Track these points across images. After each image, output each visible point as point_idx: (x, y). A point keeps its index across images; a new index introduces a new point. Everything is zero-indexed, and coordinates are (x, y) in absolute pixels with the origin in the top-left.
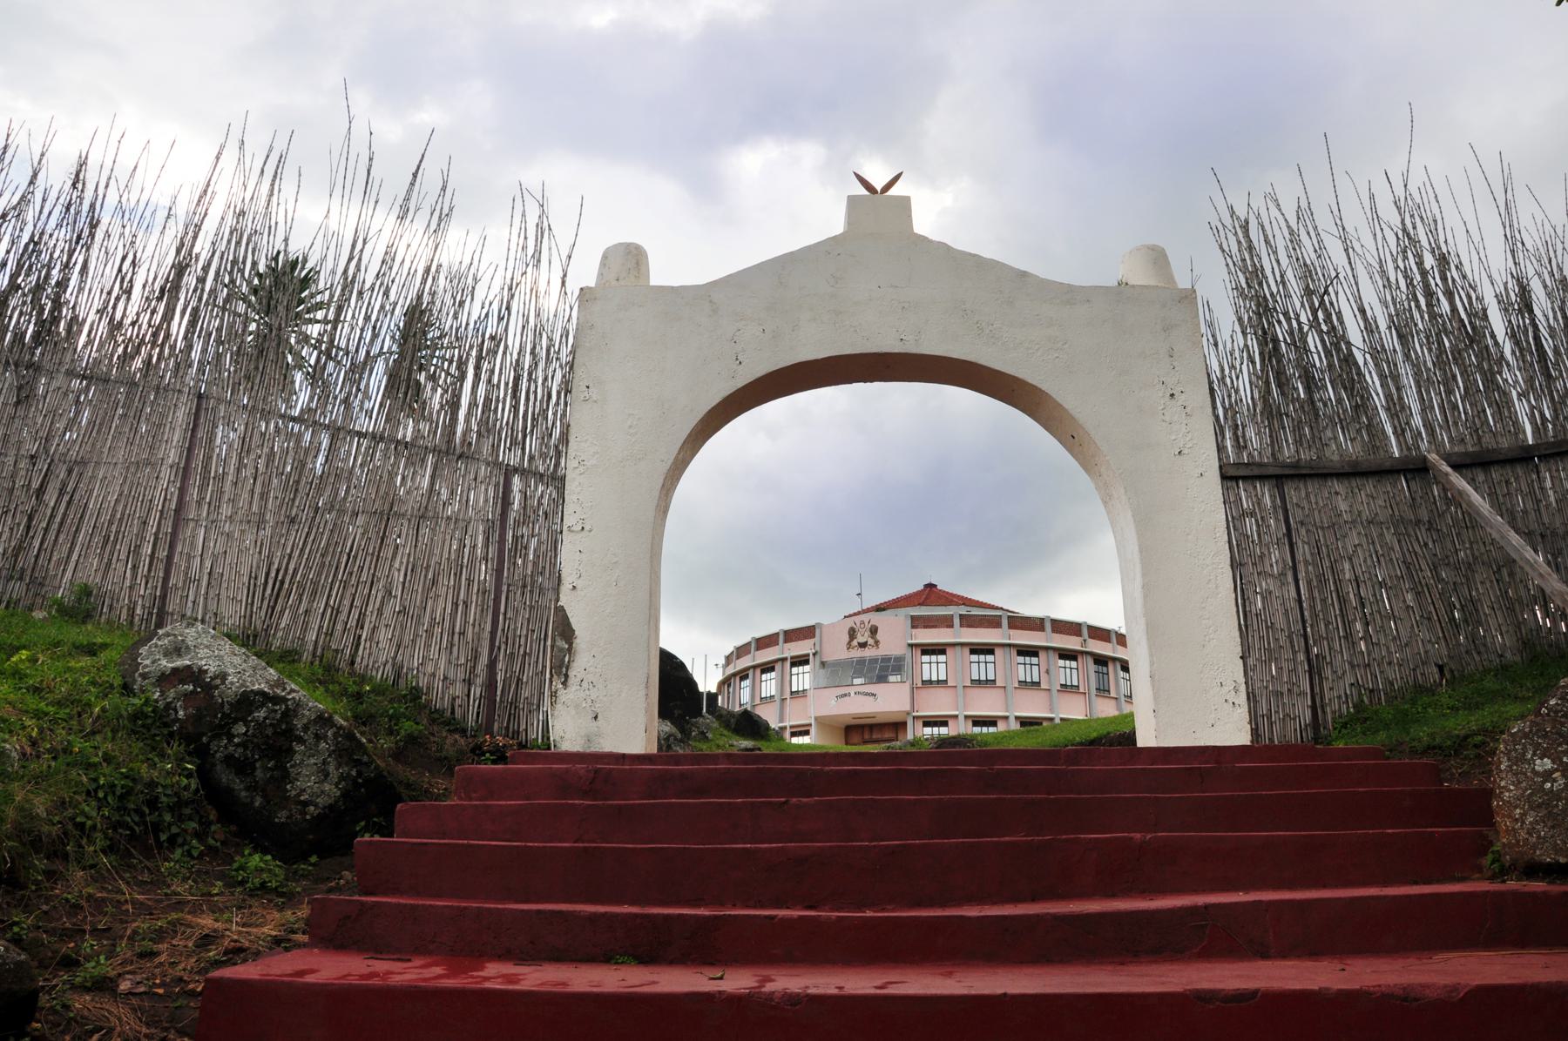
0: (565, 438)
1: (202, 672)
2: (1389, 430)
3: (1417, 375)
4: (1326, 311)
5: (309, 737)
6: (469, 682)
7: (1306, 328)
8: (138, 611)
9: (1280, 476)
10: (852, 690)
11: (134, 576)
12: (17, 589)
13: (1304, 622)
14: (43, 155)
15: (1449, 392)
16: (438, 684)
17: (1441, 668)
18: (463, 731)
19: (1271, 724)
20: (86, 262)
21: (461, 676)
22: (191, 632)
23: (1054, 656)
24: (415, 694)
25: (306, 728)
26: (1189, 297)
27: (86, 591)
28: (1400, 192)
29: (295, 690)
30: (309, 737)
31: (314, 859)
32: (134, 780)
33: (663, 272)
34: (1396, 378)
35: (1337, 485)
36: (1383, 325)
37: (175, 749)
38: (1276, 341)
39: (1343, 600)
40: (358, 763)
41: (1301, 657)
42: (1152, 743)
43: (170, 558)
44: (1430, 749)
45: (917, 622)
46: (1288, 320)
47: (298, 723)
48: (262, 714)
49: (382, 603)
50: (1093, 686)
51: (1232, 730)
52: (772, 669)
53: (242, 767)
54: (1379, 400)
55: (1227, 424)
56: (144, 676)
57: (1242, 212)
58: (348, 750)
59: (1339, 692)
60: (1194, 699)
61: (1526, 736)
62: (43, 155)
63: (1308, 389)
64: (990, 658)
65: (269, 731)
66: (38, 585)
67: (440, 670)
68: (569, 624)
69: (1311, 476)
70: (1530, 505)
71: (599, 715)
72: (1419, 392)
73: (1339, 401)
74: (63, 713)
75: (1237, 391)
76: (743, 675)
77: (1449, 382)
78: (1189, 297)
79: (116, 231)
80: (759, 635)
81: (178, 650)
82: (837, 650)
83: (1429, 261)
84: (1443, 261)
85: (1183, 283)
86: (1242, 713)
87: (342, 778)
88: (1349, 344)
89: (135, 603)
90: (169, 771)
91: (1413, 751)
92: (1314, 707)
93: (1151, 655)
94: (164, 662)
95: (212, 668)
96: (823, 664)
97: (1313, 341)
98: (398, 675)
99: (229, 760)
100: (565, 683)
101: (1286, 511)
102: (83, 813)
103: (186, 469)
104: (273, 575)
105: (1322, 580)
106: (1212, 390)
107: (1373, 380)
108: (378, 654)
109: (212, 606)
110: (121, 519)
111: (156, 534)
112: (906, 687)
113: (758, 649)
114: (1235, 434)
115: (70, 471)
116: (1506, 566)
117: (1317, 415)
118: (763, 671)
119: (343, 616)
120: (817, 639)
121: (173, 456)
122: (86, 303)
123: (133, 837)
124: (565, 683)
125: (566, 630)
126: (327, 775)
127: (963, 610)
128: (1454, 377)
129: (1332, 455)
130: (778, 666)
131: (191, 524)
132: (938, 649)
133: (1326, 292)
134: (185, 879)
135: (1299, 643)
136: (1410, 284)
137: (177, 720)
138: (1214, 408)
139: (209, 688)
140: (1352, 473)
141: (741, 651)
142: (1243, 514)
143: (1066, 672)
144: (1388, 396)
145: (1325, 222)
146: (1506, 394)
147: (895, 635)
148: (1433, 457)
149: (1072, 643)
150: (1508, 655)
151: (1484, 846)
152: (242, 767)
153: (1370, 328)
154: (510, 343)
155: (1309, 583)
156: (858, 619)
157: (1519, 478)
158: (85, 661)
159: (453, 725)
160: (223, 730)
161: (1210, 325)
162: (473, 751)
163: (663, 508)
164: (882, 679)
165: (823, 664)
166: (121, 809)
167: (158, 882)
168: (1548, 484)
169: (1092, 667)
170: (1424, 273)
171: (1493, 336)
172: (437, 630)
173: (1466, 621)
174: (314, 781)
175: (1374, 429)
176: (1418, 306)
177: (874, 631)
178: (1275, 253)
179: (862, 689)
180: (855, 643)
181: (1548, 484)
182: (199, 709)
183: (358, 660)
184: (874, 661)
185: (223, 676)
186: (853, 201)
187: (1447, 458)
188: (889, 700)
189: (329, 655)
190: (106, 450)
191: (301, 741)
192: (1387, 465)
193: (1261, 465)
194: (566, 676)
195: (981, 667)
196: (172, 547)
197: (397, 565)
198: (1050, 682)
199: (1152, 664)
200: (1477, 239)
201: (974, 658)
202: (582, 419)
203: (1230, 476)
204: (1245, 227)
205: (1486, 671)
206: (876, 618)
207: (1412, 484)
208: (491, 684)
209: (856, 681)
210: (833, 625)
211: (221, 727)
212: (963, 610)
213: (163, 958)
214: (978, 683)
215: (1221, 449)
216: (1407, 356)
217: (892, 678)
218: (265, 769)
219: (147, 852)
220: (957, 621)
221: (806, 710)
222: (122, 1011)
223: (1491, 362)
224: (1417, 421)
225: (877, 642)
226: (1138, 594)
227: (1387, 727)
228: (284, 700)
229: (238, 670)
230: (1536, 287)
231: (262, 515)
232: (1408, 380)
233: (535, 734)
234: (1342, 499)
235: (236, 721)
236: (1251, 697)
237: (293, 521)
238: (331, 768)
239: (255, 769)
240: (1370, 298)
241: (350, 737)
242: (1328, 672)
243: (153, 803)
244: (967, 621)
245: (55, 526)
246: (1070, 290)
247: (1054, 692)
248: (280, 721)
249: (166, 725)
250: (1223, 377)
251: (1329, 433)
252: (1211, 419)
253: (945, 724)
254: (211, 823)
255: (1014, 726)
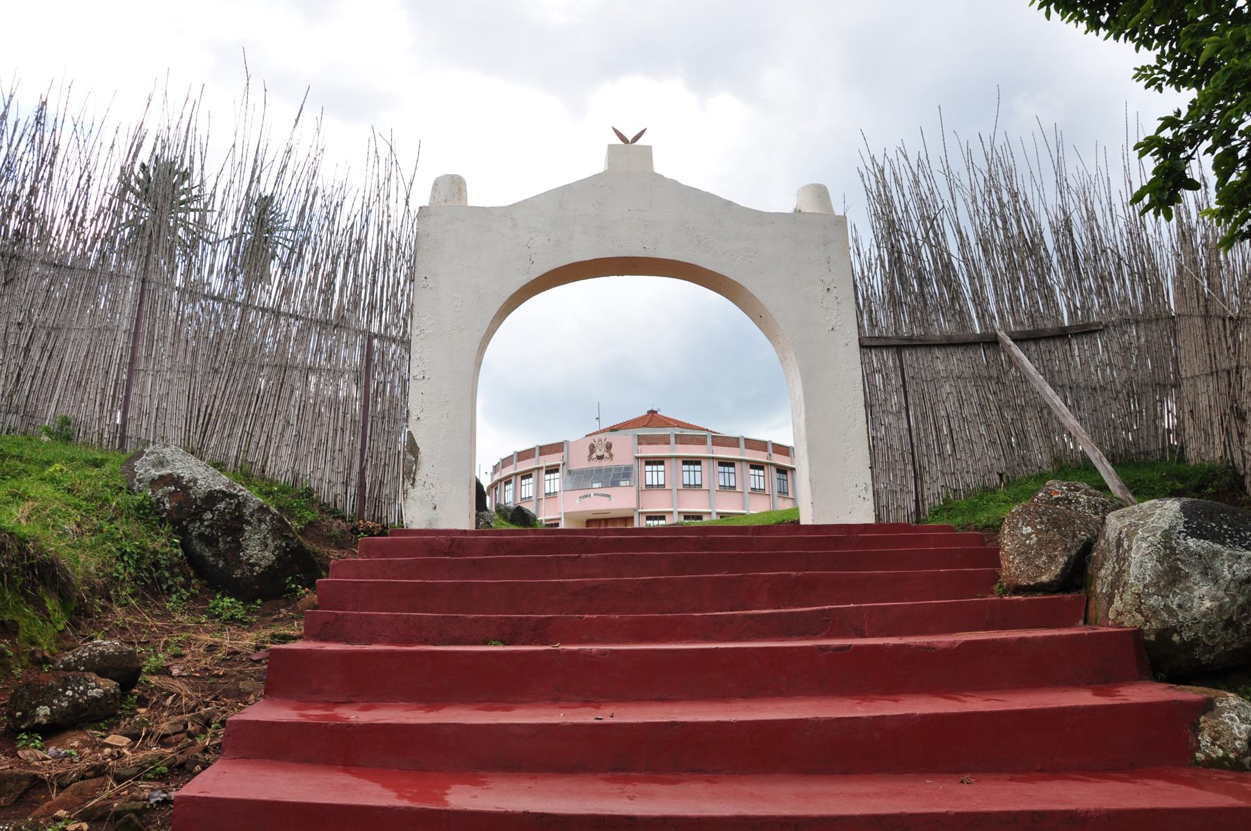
0: (410, 311)
1: (180, 478)
2: (974, 315)
3: (994, 277)
4: (934, 232)
5: (254, 521)
6: (346, 484)
7: (920, 243)
8: (106, 435)
9: (899, 346)
10: (592, 492)
11: (101, 411)
12: (13, 420)
13: (912, 444)
14: (11, 96)
15: (1015, 289)
16: (325, 486)
17: (1001, 475)
18: (344, 518)
19: (888, 512)
20: (51, 174)
21: (340, 480)
22: (167, 450)
23: (746, 467)
24: (309, 492)
25: (252, 515)
26: (842, 221)
27: (66, 422)
28: (988, 149)
29: (242, 490)
30: (254, 521)
31: (259, 601)
32: (144, 550)
33: (476, 197)
34: (981, 278)
35: (937, 352)
36: (973, 242)
37: (168, 528)
38: (900, 252)
39: (938, 430)
40: (287, 538)
41: (910, 467)
42: (810, 523)
43: (127, 398)
44: (986, 526)
45: (642, 440)
46: (909, 237)
47: (247, 512)
48: (222, 506)
49: (283, 430)
50: (776, 489)
51: (863, 514)
52: (530, 476)
53: (210, 541)
54: (968, 295)
55: (864, 308)
56: (140, 481)
57: (880, 161)
58: (280, 529)
59: (934, 492)
60: (837, 493)
61: (1019, 514)
62: (11, 96)
63: (920, 285)
64: (698, 468)
65: (228, 517)
66: (29, 417)
67: (328, 478)
68: (415, 444)
69: (920, 346)
70: (1064, 367)
71: (434, 505)
72: (995, 289)
73: (941, 294)
74: (91, 506)
75: (872, 287)
76: (507, 480)
77: (1014, 281)
78: (842, 221)
79: (73, 156)
80: (519, 450)
81: (161, 463)
82: (580, 461)
83: (1006, 198)
84: (1015, 195)
85: (838, 211)
86: (870, 504)
87: (276, 548)
88: (949, 255)
89: (103, 430)
90: (163, 544)
91: (976, 529)
92: (917, 501)
93: (810, 466)
94: (153, 471)
95: (187, 475)
96: (570, 472)
97: (925, 252)
98: (296, 479)
99: (201, 536)
100: (413, 485)
101: (902, 370)
102: (117, 571)
103: (136, 334)
104: (203, 409)
105: (925, 416)
106: (855, 286)
107: (964, 280)
108: (281, 466)
109: (160, 432)
110: (89, 370)
111: (116, 381)
112: (634, 490)
113: (519, 460)
114: (870, 317)
115: (49, 334)
116: (1044, 409)
117: (926, 304)
118: (523, 478)
119: (255, 439)
120: (565, 452)
121: (125, 324)
122: (55, 208)
123: (146, 587)
124: (413, 485)
125: (413, 448)
126: (266, 546)
127: (678, 431)
128: (1019, 279)
129: (935, 332)
130: (535, 474)
131: (142, 374)
132: (658, 461)
133: (935, 218)
134: (182, 614)
135: (908, 458)
136: (993, 214)
137: (165, 510)
138: (857, 298)
139: (186, 489)
140: (948, 344)
141: (506, 462)
142: (874, 371)
143: (755, 479)
144: (975, 292)
145: (936, 166)
146: (1051, 290)
147: (625, 450)
148: (1002, 334)
149: (760, 457)
150: (1045, 467)
151: (995, 578)
152: (210, 541)
153: (963, 243)
154: (369, 245)
155: (916, 418)
156: (596, 437)
157: (1058, 349)
158: (96, 471)
159: (338, 515)
160: (197, 516)
161: (856, 241)
162: (351, 531)
163: (478, 364)
164: (615, 484)
165: (570, 472)
166: (138, 568)
167: (167, 615)
168: (1076, 352)
169: (775, 475)
170: (1002, 206)
171: (1045, 249)
172: (323, 448)
173: (1018, 444)
174: (258, 550)
175: (962, 314)
176: (997, 226)
177: (609, 447)
178: (902, 189)
179: (599, 491)
180: (594, 456)
181: (1076, 352)
182: (180, 503)
183: (267, 469)
184: (608, 470)
185: (195, 481)
186: (611, 148)
187: (1011, 335)
188: (619, 501)
189: (247, 467)
190: (75, 319)
191: (249, 523)
192: (971, 339)
193: (886, 338)
194: (414, 479)
195: (690, 475)
196: (128, 390)
197: (292, 403)
198: (743, 487)
199: (811, 472)
200: (1039, 183)
201: (686, 467)
202: (423, 302)
203: (866, 346)
204: (882, 171)
205: (1030, 478)
206: (611, 437)
207: (988, 352)
208: (362, 485)
209: (595, 485)
210: (577, 441)
211: (195, 514)
212: (678, 431)
213: (189, 657)
214: (688, 487)
215: (860, 327)
216: (988, 263)
217: (622, 483)
218: (225, 542)
219: (156, 596)
220: (672, 440)
221: (559, 504)
222: (177, 683)
223: (1042, 267)
224: (993, 308)
225: (611, 456)
226: (802, 425)
227: (963, 514)
228: (236, 496)
229: (205, 478)
230: (1075, 218)
231: (193, 367)
232: (988, 281)
233: (392, 520)
234: (941, 362)
235: (205, 511)
236: (876, 494)
237: (216, 371)
238: (269, 541)
239: (218, 542)
240: (965, 224)
241: (281, 520)
242: (927, 478)
243: (156, 564)
244: (681, 440)
245: (40, 375)
246: (760, 214)
247: (746, 494)
248: (235, 510)
249: (157, 513)
250: (863, 277)
251: (934, 317)
252: (855, 306)
253: (663, 518)
254: (191, 579)
255: (714, 517)
